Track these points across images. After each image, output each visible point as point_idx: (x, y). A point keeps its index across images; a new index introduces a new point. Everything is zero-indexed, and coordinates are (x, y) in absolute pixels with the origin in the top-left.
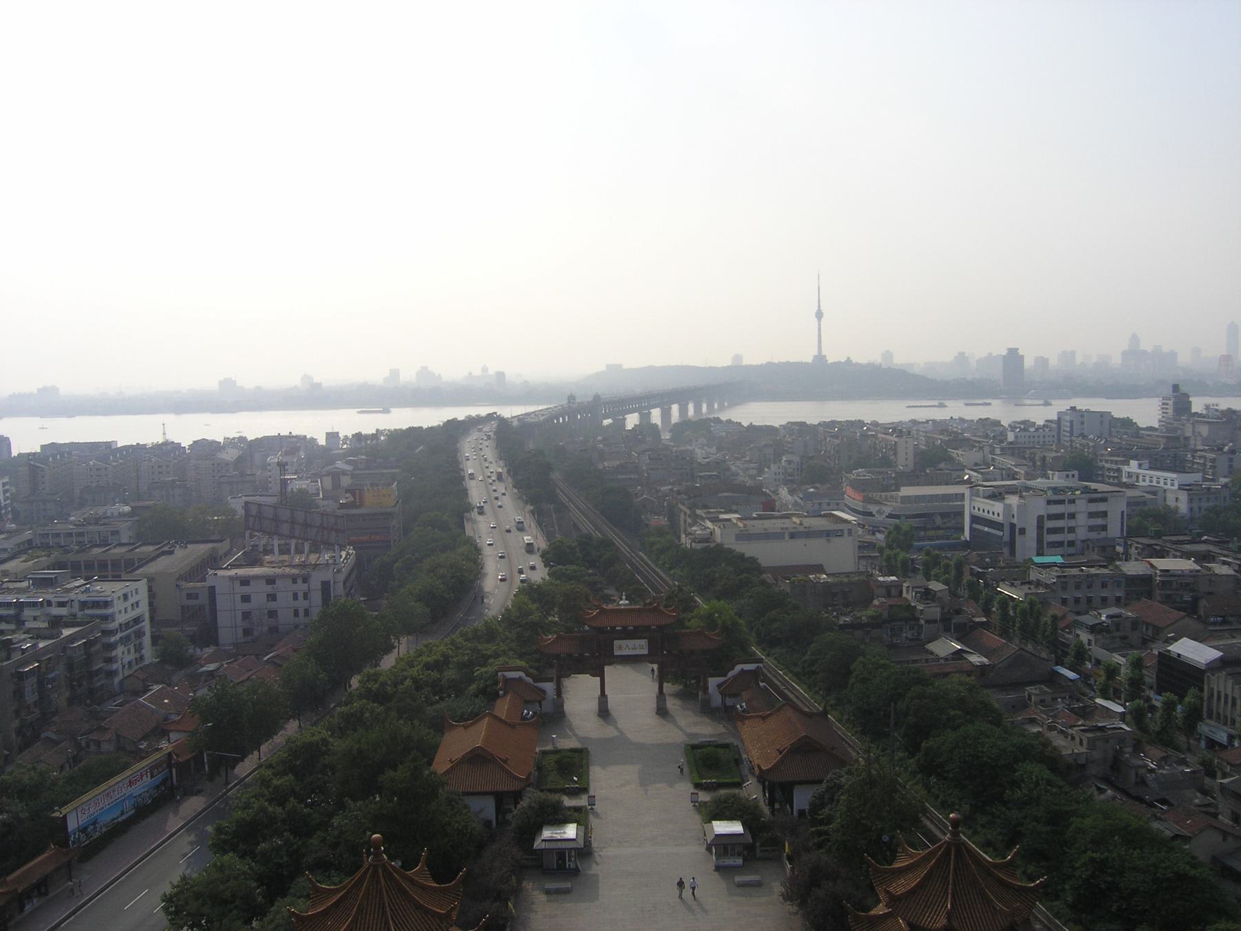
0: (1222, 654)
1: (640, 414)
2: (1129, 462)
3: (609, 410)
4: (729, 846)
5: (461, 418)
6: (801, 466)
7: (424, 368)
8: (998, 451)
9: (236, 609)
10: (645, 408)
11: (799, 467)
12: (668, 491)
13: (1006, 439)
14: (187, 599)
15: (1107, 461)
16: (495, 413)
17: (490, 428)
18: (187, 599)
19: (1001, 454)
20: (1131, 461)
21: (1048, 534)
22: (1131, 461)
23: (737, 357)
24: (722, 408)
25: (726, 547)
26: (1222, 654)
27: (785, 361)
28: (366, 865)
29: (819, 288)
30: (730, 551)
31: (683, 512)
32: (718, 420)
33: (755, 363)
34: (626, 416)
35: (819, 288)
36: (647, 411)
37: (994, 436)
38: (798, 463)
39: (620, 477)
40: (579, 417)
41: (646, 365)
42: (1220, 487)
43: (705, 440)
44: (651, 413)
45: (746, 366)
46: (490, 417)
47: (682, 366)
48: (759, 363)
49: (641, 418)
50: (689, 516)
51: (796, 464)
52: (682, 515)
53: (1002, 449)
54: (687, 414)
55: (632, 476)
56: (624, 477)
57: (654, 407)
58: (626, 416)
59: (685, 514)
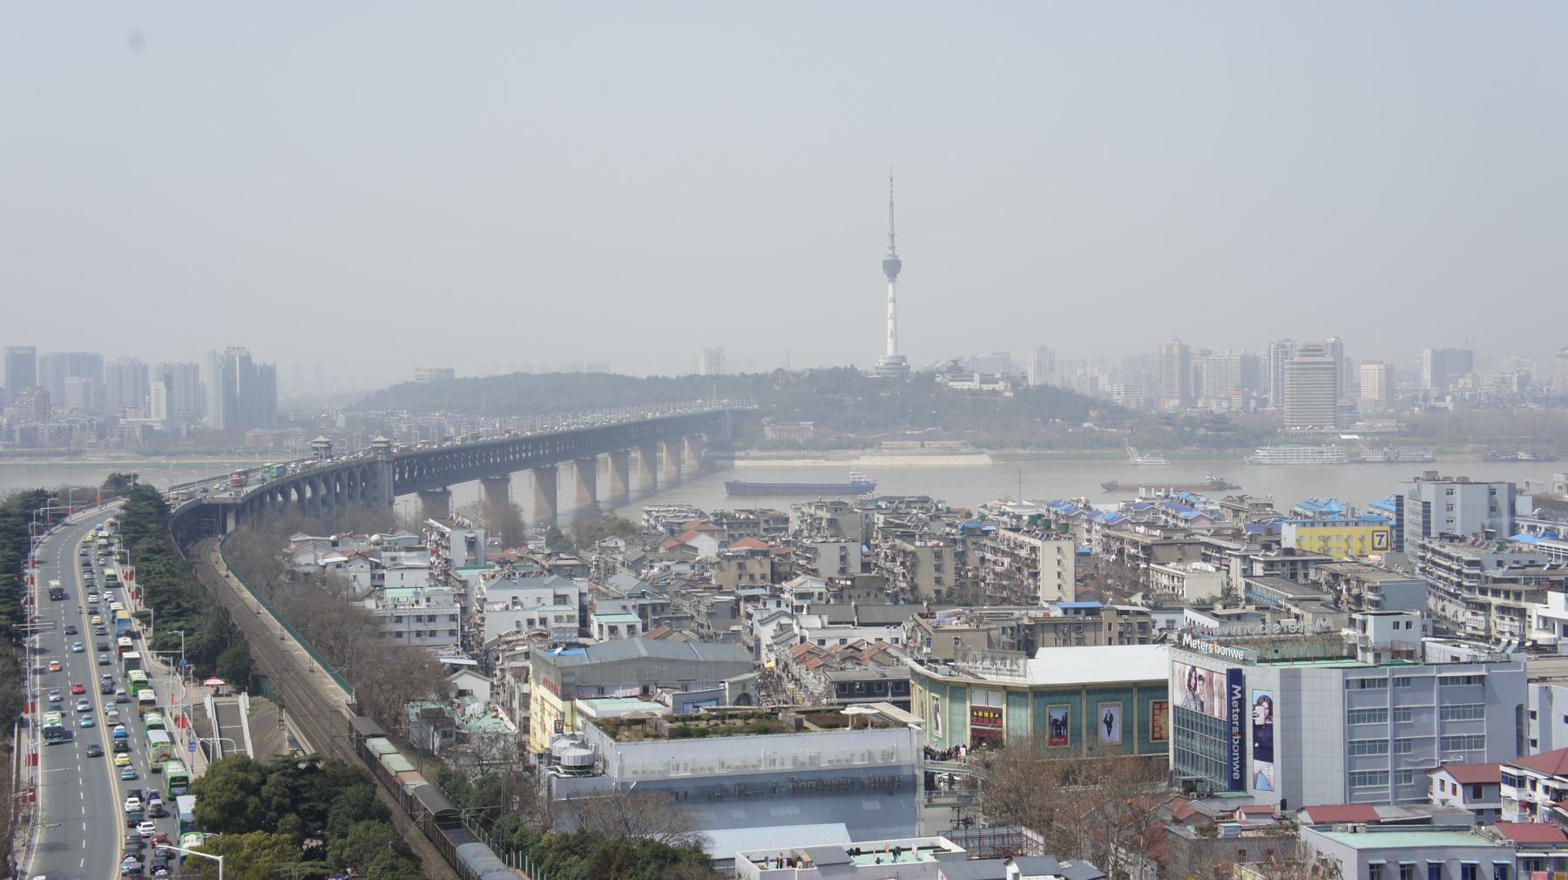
2: (1546, 595)
3: (411, 474)
8: (1258, 570)
13: (1278, 543)
14: (555, 603)
15: (1496, 593)
18: (555, 603)
19: (1266, 575)
20: (1550, 594)
21: (1556, 652)
22: (1550, 594)
27: (830, 366)
28: (1471, 652)
29: (892, 203)
34: (449, 488)
35: (892, 203)
36: (623, 450)
37: (1251, 536)
40: (492, 461)
44: (449, 493)
53: (1270, 565)
57: (520, 465)
58: (449, 488)
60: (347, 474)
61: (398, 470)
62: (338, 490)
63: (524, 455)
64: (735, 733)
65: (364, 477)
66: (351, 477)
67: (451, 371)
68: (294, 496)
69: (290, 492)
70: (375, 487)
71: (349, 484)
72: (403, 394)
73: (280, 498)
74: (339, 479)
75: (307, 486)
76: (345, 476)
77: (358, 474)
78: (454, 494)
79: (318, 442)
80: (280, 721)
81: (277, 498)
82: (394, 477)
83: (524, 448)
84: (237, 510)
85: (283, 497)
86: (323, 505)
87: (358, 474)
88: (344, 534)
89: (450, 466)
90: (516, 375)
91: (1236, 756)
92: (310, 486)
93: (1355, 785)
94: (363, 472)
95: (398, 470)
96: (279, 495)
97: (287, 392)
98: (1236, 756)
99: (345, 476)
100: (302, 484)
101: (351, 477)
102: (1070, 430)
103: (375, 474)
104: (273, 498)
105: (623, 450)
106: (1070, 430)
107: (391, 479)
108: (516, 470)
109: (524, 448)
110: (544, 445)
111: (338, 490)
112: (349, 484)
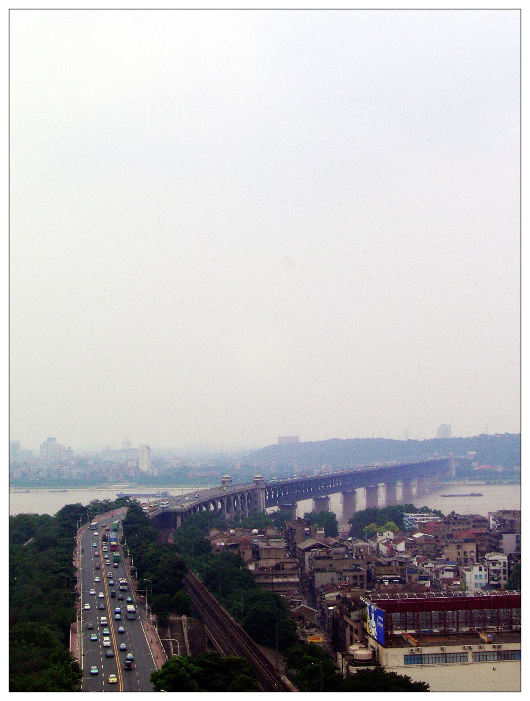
0: (413, 536)
5: (85, 503)
6: (509, 567)
7: (51, 440)
9: (482, 657)
11: (507, 568)
12: (334, 599)
17: (122, 513)
23: (445, 428)
24: (421, 494)
25: (388, 671)
26: (413, 536)
30: (393, 674)
31: (349, 627)
32: (411, 509)
33: (464, 436)
36: (324, 496)
38: (504, 563)
39: (275, 580)
41: (328, 438)
42: (161, 690)
43: (391, 534)
45: (454, 439)
46: (122, 501)
47: (374, 440)
48: (471, 436)
51: (502, 564)
52: (348, 630)
54: (377, 501)
55: (292, 580)
56: (280, 580)
57: (334, 490)
60: (247, 494)
61: (268, 493)
62: (236, 504)
63: (337, 484)
66: (243, 498)
67: (298, 438)
68: (212, 508)
69: (210, 505)
70: (256, 503)
71: (241, 501)
72: (266, 452)
73: (204, 509)
74: (236, 498)
76: (239, 497)
77: (246, 495)
78: (331, 499)
79: (225, 478)
81: (203, 509)
82: (266, 497)
83: (334, 481)
84: (182, 515)
85: (206, 508)
86: (227, 513)
87: (246, 495)
93: (485, 626)
94: (249, 495)
96: (204, 507)
97: (56, 514)
99: (239, 497)
100: (216, 501)
101: (243, 498)
102: (16, 579)
103: (255, 495)
105: (324, 496)
106: (16, 579)
108: (300, 500)
109: (334, 481)
110: (335, 481)
111: (236, 504)
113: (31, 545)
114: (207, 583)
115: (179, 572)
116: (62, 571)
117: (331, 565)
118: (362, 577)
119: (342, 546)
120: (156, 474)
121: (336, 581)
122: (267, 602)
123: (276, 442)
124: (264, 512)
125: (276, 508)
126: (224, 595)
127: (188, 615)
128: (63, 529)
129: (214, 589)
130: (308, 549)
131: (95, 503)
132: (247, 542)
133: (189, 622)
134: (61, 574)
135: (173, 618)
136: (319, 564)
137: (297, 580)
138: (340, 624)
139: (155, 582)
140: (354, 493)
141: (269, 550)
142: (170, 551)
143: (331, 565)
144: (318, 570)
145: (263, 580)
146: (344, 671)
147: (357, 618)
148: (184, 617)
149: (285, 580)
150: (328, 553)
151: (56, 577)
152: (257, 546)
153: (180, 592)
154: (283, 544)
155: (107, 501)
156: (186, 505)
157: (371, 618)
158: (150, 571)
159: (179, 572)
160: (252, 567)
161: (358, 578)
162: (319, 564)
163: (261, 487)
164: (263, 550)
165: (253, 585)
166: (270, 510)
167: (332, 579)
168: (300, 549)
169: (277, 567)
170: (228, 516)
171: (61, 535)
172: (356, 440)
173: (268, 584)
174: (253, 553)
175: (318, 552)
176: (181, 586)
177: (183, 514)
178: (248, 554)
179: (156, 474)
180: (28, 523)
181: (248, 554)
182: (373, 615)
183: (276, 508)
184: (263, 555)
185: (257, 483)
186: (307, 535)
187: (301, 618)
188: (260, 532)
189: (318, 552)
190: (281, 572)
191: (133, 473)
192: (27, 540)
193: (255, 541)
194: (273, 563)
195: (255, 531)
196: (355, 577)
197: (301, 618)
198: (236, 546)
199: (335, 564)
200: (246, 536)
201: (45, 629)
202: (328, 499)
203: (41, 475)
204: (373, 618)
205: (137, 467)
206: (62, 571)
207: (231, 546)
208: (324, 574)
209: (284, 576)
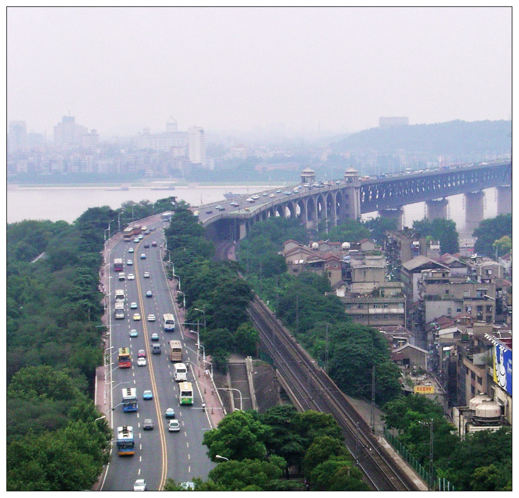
1: (430, 203)
4: (243, 229)
7: (69, 120)
10: (438, 193)
16: (173, 199)
36: (440, 199)
39: (372, 311)
49: (431, 211)
50: (480, 380)
52: (468, 378)
55: (394, 310)
56: (379, 311)
57: (454, 191)
59: (473, 375)
61: (364, 194)
62: (320, 209)
64: (92, 397)
65: (339, 199)
66: (330, 199)
68: (288, 213)
69: (275, 212)
70: (347, 206)
73: (277, 214)
74: (320, 200)
75: (287, 208)
77: (334, 196)
80: (274, 378)
85: (280, 213)
87: (334, 196)
88: (323, 242)
89: (409, 190)
90: (417, 124)
91: (129, 393)
92: (300, 206)
95: (364, 194)
96: (277, 212)
98: (129, 393)
101: (330, 199)
103: (347, 196)
104: (273, 214)
105: (440, 199)
107: (359, 200)
110: (461, 177)
111: (320, 209)
112: (337, 205)
113: (41, 262)
114: (280, 314)
115: (242, 299)
116: (84, 297)
117: (447, 292)
118: (488, 307)
119: (464, 266)
120: (212, 167)
121: (454, 314)
122: (359, 340)
123: (375, 124)
124: (359, 219)
125: (374, 215)
126: (302, 331)
127: (254, 355)
128: (85, 241)
129: (290, 322)
130: (418, 270)
131: (128, 206)
132: (336, 260)
133: (256, 366)
134: (81, 301)
135: (234, 360)
136: (432, 289)
137: (402, 311)
138: (458, 370)
139: (210, 312)
140: (481, 195)
141: (364, 270)
142: (229, 270)
143: (447, 292)
144: (430, 298)
145: (355, 310)
146: (463, 432)
147: (480, 362)
148: (249, 360)
149: (386, 311)
150: (444, 275)
151: (76, 306)
152: (348, 265)
153: (243, 326)
154: (384, 263)
155: (144, 203)
156: (253, 209)
157: (499, 363)
158: (203, 298)
159: (242, 299)
160: (341, 293)
161: (485, 309)
162: (432, 289)
163: (355, 185)
164: (357, 271)
165: (342, 317)
166: (367, 217)
167: (449, 309)
168: (406, 269)
169: (375, 293)
170: (309, 225)
171: (82, 249)
172: (487, 123)
173: (363, 315)
174: (343, 274)
175: (430, 273)
176: (245, 318)
177: (248, 221)
178: (336, 277)
179: (212, 167)
180: (39, 233)
181: (336, 277)
182: (502, 358)
183: (374, 215)
184: (357, 276)
185: (350, 180)
186: (416, 251)
187: (406, 361)
188: (353, 247)
189: (430, 273)
190: (379, 300)
191: (180, 167)
192: (36, 256)
193: (346, 258)
194: (369, 287)
195: (346, 244)
196: (480, 308)
197: (406, 361)
198: (320, 265)
199: (452, 290)
200: (334, 252)
201: (61, 375)
202: (445, 203)
203: (54, 167)
204: (502, 362)
205: (187, 157)
206: (84, 297)
207: (313, 265)
208: (438, 303)
209: (385, 305)
